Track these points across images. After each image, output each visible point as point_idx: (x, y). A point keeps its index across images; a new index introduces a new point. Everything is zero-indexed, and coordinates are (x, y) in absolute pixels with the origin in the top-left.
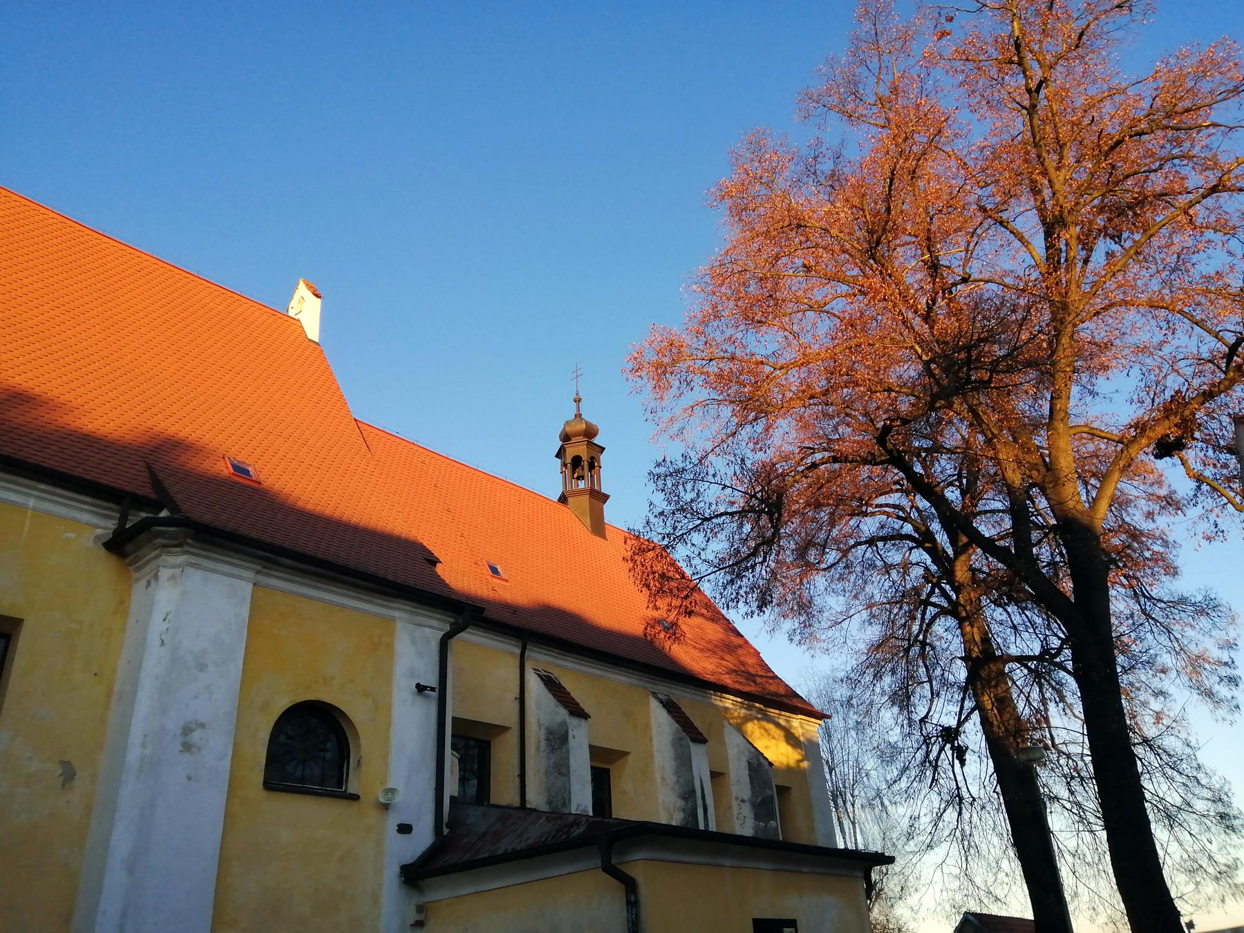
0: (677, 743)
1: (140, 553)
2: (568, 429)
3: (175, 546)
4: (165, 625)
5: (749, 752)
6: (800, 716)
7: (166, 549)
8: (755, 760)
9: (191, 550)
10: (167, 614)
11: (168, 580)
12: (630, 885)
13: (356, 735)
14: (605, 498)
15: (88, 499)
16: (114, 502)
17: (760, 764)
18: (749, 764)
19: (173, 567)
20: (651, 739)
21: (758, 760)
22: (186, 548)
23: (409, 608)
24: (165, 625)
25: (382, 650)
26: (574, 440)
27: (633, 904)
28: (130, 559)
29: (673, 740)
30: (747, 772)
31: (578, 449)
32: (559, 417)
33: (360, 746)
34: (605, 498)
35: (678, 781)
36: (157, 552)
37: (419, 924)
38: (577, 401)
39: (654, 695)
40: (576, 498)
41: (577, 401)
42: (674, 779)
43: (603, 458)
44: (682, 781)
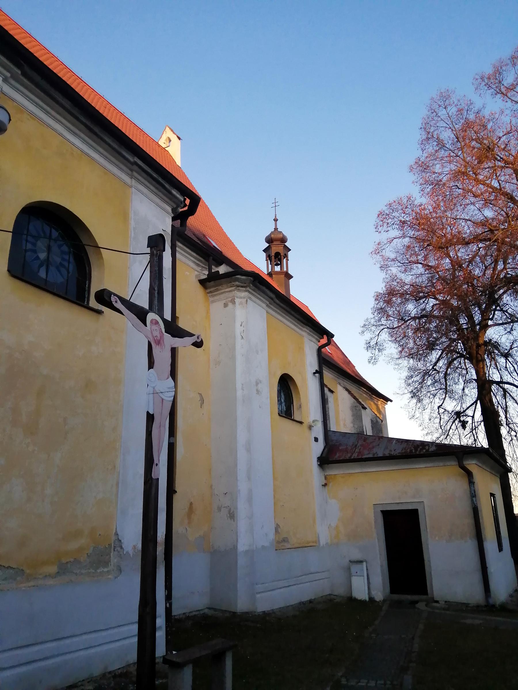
0: (354, 408)
1: (220, 287)
2: (272, 236)
3: (242, 287)
4: (242, 328)
5: (372, 415)
6: (382, 400)
7: (238, 288)
8: (375, 419)
9: (250, 290)
10: (242, 323)
11: (240, 304)
12: (469, 474)
13: (298, 393)
14: (291, 277)
15: (195, 254)
16: (204, 258)
17: (377, 421)
18: (372, 421)
19: (241, 298)
20: (338, 405)
21: (376, 419)
22: (248, 289)
23: (308, 331)
24: (242, 328)
25: (301, 349)
26: (275, 243)
27: (471, 482)
28: (208, 291)
29: (351, 406)
30: (370, 425)
31: (276, 248)
32: (269, 230)
33: (300, 398)
34: (291, 277)
35: (354, 426)
36: (233, 288)
37: (325, 485)
38: (276, 220)
39: (340, 384)
40: (277, 276)
41: (276, 220)
42: (352, 425)
43: (290, 253)
44: (356, 426)
